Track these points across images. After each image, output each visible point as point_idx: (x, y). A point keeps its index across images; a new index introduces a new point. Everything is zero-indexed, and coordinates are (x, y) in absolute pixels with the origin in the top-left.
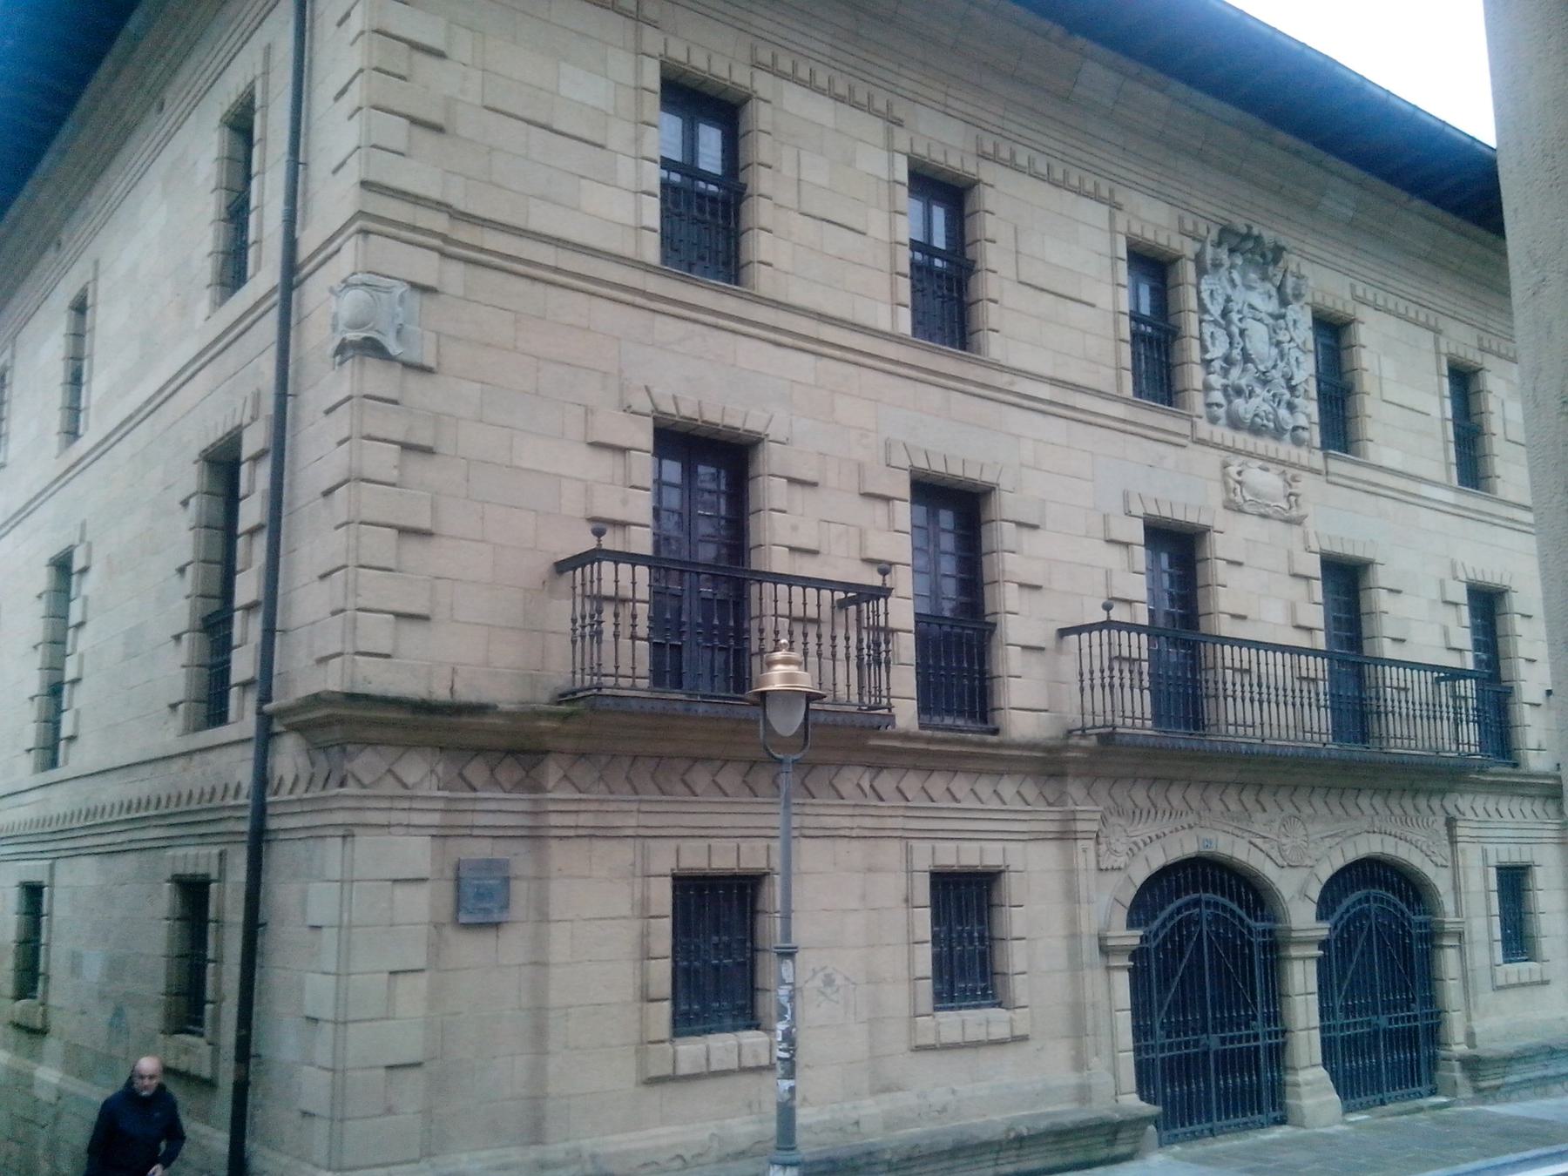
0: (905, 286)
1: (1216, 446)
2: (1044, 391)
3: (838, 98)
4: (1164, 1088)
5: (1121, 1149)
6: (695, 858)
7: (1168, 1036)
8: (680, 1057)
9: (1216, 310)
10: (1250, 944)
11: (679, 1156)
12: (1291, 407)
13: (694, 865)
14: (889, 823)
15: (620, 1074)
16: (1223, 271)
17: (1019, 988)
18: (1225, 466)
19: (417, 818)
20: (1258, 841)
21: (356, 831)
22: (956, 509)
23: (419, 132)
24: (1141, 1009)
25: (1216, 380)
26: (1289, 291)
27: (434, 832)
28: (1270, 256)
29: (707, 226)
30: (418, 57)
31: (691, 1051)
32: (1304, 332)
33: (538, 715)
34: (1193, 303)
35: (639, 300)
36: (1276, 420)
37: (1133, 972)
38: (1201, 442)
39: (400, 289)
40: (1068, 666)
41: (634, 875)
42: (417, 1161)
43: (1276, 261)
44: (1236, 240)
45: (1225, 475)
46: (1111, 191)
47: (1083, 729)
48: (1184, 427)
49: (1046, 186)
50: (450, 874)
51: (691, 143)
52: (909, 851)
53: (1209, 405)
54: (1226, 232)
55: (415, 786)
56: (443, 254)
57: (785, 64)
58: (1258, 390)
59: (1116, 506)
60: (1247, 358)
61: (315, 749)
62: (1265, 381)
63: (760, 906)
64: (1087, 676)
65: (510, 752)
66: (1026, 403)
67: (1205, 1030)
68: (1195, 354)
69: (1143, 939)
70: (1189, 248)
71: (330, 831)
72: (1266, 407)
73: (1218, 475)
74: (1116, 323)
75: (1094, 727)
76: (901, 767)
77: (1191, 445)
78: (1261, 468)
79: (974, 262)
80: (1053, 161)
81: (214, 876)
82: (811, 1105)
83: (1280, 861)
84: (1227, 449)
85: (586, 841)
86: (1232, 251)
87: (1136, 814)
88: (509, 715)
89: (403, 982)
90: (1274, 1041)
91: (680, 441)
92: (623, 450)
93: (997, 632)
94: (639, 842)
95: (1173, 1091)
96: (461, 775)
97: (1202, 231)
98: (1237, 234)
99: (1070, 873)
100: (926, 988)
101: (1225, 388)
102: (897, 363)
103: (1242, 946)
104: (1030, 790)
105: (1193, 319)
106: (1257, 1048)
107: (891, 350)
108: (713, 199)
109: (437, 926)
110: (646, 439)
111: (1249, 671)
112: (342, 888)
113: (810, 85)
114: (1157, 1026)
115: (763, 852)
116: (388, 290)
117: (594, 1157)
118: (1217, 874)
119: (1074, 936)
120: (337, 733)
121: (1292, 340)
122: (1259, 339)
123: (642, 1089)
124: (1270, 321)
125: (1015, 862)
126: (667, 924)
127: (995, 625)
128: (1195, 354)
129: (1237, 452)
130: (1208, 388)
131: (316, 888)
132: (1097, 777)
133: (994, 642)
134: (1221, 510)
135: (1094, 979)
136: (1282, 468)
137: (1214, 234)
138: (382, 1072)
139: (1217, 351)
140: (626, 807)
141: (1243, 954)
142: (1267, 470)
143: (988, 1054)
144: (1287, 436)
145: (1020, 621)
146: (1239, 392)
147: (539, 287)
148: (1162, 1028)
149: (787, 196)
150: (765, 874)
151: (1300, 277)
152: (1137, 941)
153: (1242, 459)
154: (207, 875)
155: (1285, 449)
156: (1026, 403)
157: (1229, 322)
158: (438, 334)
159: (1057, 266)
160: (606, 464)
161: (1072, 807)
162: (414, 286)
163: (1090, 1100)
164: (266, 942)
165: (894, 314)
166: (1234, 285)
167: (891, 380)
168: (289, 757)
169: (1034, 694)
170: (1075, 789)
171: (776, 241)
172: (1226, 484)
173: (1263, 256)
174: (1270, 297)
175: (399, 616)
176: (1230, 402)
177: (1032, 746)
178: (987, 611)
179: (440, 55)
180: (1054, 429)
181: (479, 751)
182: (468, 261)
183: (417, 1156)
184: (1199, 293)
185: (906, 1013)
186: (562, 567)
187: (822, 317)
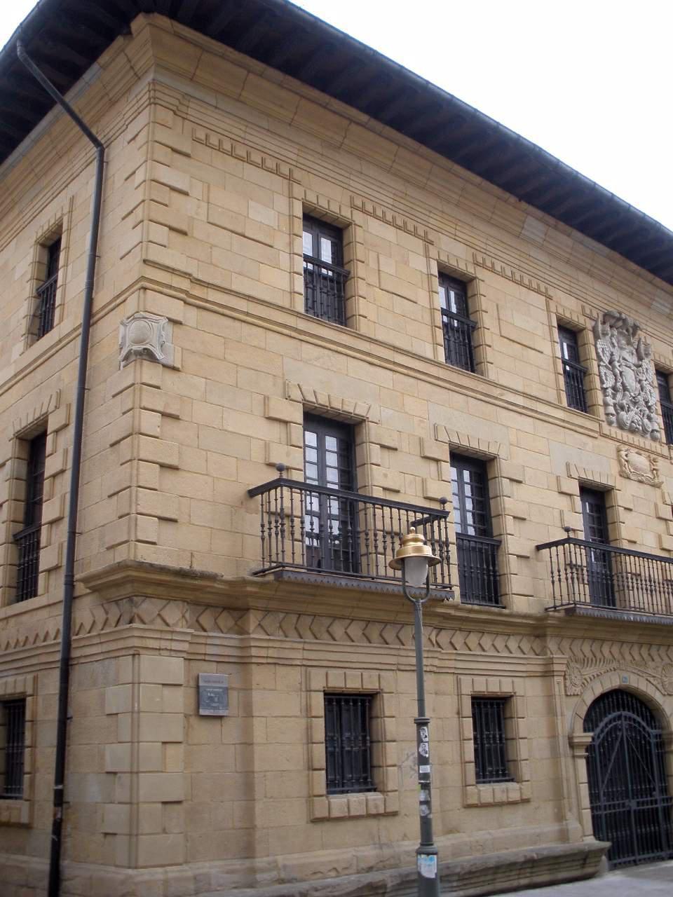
0: (440, 334)
1: (612, 439)
2: (520, 400)
3: (399, 228)
4: (607, 833)
5: (589, 870)
6: (337, 681)
7: (609, 801)
8: (333, 806)
9: (606, 360)
10: (649, 743)
11: (335, 869)
12: (649, 418)
13: (337, 685)
14: (447, 664)
15: (295, 815)
16: (608, 337)
17: (525, 770)
18: (619, 451)
19: (175, 646)
20: (651, 679)
21: (141, 651)
22: (476, 467)
23: (174, 234)
24: (593, 783)
25: (610, 400)
26: (642, 351)
27: (185, 655)
28: (631, 330)
29: (331, 293)
30: (175, 195)
31: (339, 803)
32: (651, 376)
33: (244, 582)
34: (594, 356)
35: (293, 334)
36: (643, 425)
37: (587, 759)
38: (605, 436)
39: (164, 321)
40: (543, 569)
41: (301, 690)
42: (180, 864)
43: (634, 334)
44: (612, 320)
45: (619, 456)
46: (546, 289)
47: (555, 607)
48: (595, 426)
49: (511, 283)
50: (192, 683)
51: (317, 247)
52: (458, 682)
53: (607, 414)
54: (607, 316)
55: (174, 625)
56: (185, 302)
57: (369, 208)
58: (632, 407)
59: (562, 472)
60: (625, 389)
61: (107, 602)
62: (635, 403)
63: (374, 714)
64: (556, 573)
65: (225, 608)
66: (511, 407)
67: (627, 797)
68: (598, 385)
69: (593, 738)
70: (589, 324)
71: (124, 652)
72: (637, 417)
73: (614, 455)
74: (555, 364)
75: (562, 605)
76: (452, 629)
77: (600, 437)
78: (637, 453)
79: (476, 323)
80: (514, 270)
81: (29, 691)
82: (409, 839)
83: (663, 691)
84: (618, 441)
85: (272, 666)
86: (611, 327)
87: (584, 662)
88: (226, 582)
89: (171, 749)
90: (665, 804)
91: (318, 419)
92: (286, 423)
93: (502, 546)
94: (303, 668)
95: (613, 835)
96: (197, 621)
97: (595, 315)
98: (614, 317)
99: (550, 697)
100: (471, 768)
101: (615, 405)
102: (438, 379)
103: (645, 744)
104: (526, 646)
105: (595, 363)
106: (657, 809)
107: (434, 370)
108: (331, 280)
109: (186, 716)
110: (299, 417)
111: (640, 575)
112: (139, 679)
113: (383, 219)
114: (602, 793)
115: (377, 678)
116: (157, 321)
117: (285, 867)
118: (630, 699)
119: (553, 736)
120: (128, 590)
121: (646, 380)
122: (630, 378)
123: (311, 825)
124: (633, 368)
125: (520, 692)
126: (322, 721)
127: (500, 542)
128: (598, 385)
129: (624, 443)
130: (606, 405)
131: (111, 690)
132: (563, 637)
133: (500, 553)
134: (618, 476)
135: (566, 762)
136: (647, 454)
137: (601, 318)
138: (160, 806)
139: (609, 383)
140: (296, 645)
141: (646, 750)
142: (640, 454)
143: (507, 811)
144: (648, 436)
145: (516, 541)
146: (622, 408)
147: (237, 324)
148: (604, 795)
149: (373, 279)
150: (378, 693)
151: (646, 345)
152: (590, 740)
153: (627, 447)
154: (23, 693)
155: (647, 443)
156: (511, 407)
157: (614, 367)
158: (182, 349)
159: (522, 332)
160: (276, 431)
161: (549, 655)
162: (170, 320)
163: (568, 839)
164: (73, 729)
165: (435, 351)
166: (614, 346)
167: (438, 389)
168: (86, 611)
169: (529, 586)
170: (552, 644)
171: (367, 303)
172: (620, 461)
173: (627, 330)
174: (633, 354)
175: (160, 518)
176: (618, 413)
177: (525, 616)
178: (495, 534)
179: (186, 194)
180: (526, 423)
181: (208, 606)
182: (199, 307)
183: (181, 860)
184: (596, 349)
185: (459, 784)
186: (252, 493)
187: (396, 349)
